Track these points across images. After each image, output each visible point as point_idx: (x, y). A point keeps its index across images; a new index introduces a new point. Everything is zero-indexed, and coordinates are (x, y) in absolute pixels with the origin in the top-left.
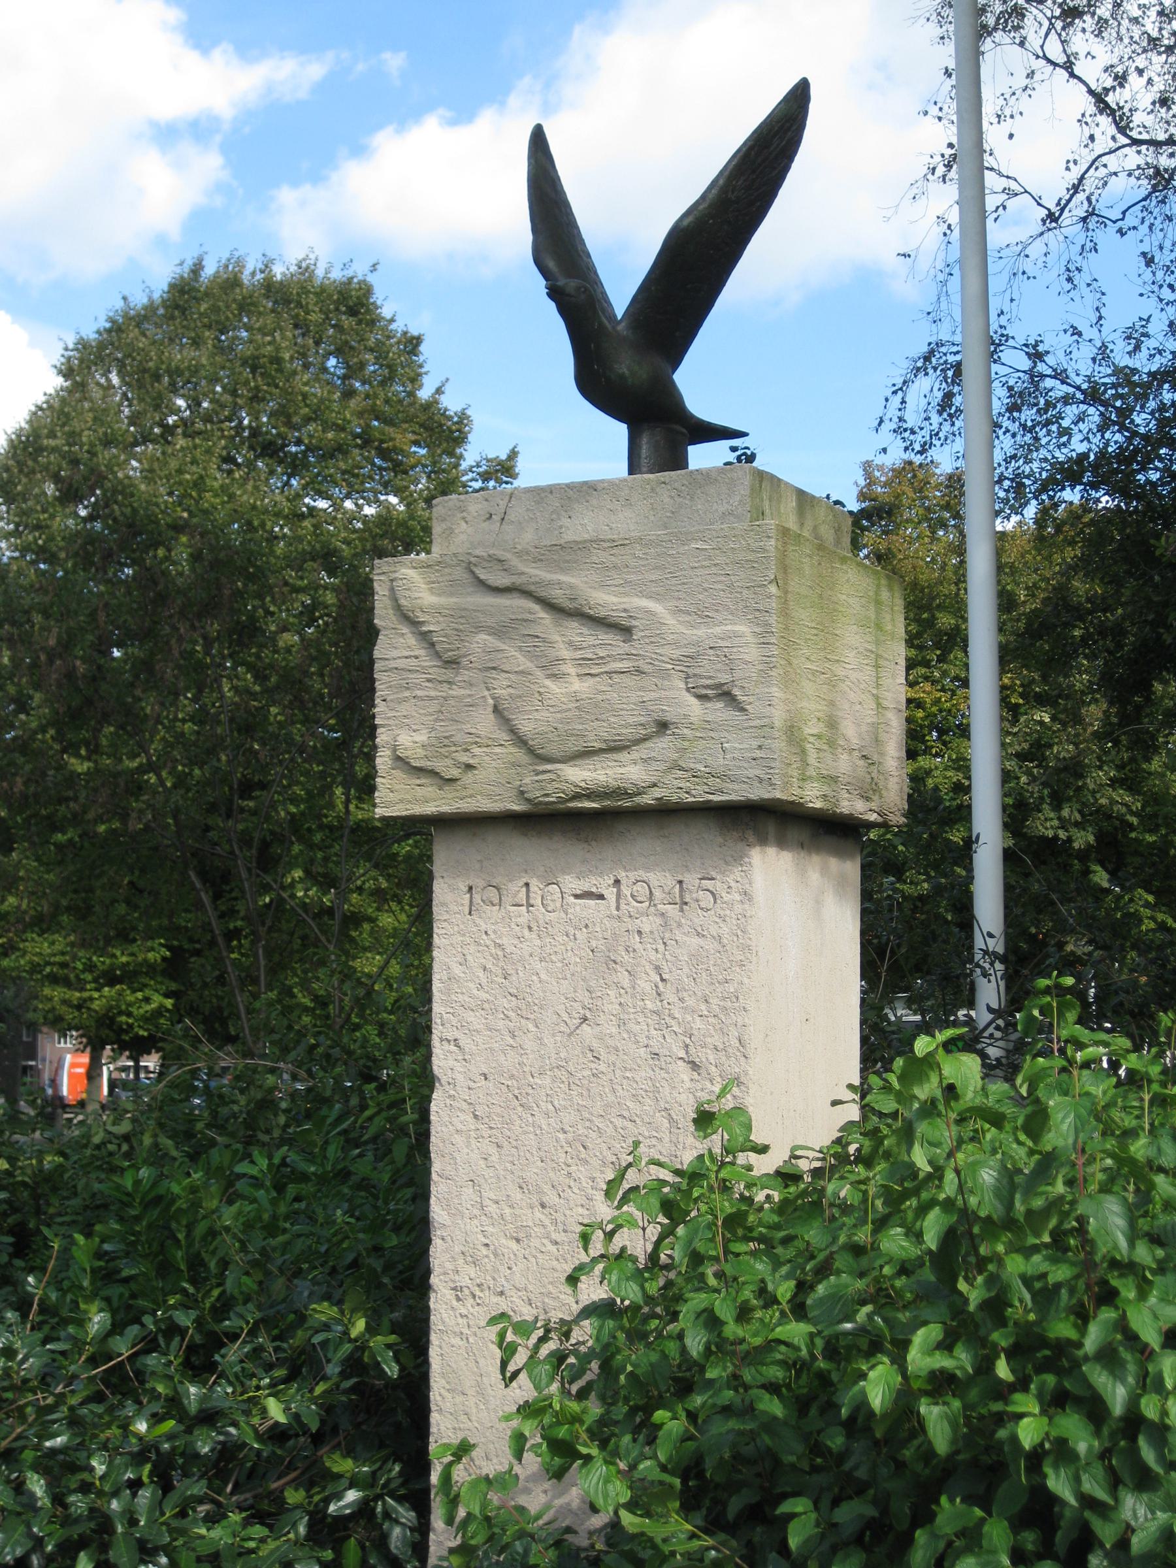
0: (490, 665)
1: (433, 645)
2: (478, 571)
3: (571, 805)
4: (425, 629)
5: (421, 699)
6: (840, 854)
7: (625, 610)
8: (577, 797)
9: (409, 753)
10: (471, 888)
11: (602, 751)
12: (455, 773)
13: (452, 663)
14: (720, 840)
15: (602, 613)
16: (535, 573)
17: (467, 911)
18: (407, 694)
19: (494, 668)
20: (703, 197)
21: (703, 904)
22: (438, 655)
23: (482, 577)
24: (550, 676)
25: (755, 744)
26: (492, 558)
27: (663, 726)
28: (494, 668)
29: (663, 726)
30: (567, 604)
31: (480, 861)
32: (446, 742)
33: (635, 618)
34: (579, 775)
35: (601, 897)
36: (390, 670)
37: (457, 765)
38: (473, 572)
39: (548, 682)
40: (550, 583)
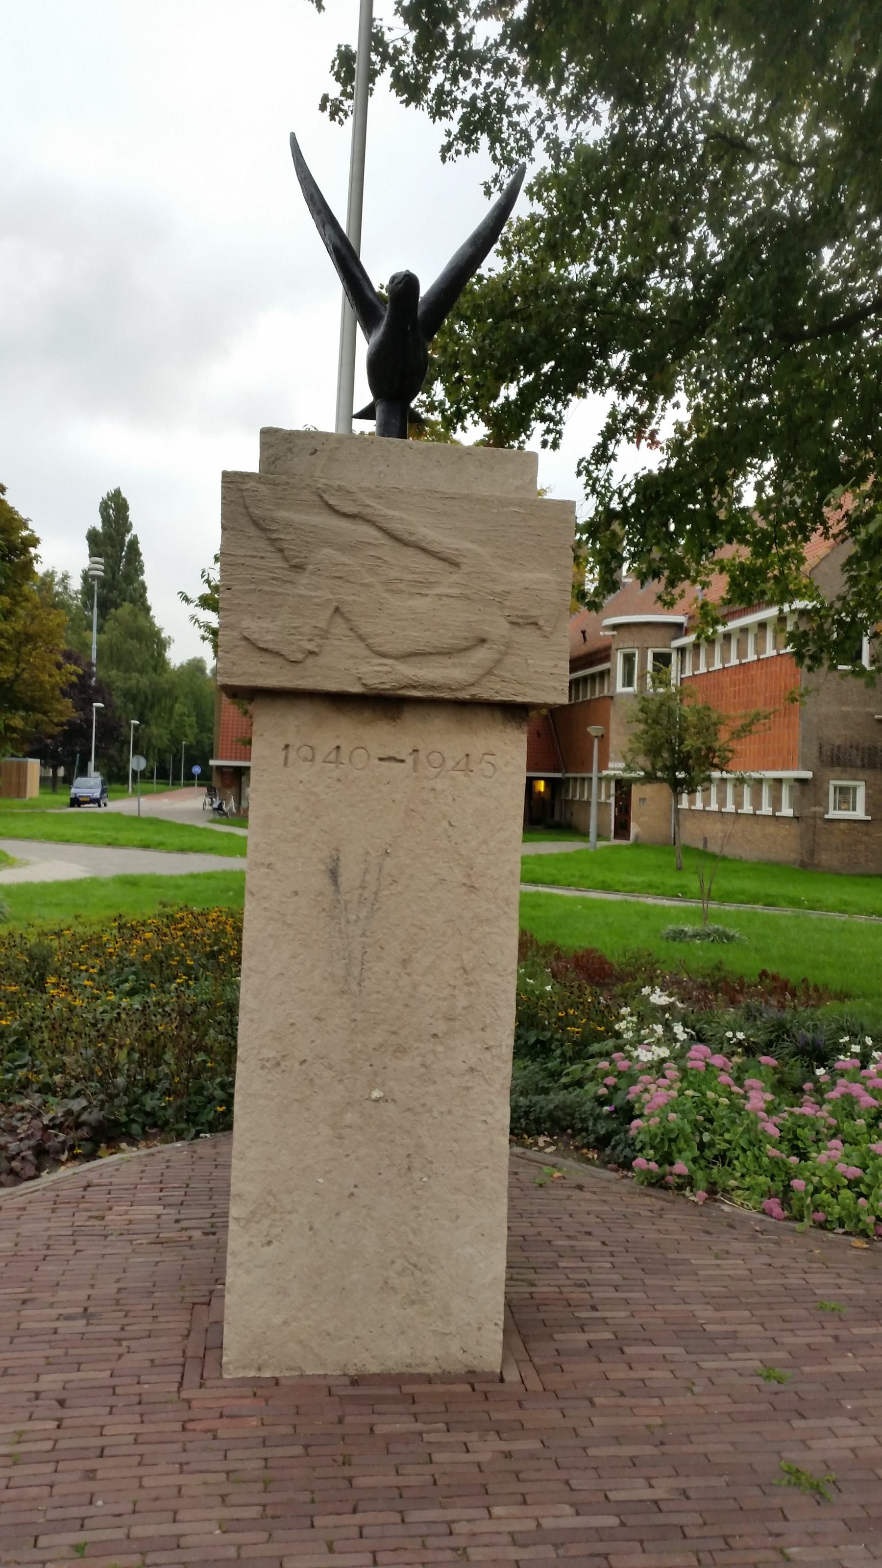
0: (337, 575)
1: (281, 550)
2: (326, 497)
3: (400, 692)
4: (274, 536)
5: (267, 593)
6: (520, 727)
7: (457, 550)
8: (404, 687)
9: (256, 636)
10: (287, 746)
11: (431, 654)
12: (300, 656)
13: (299, 568)
14: (501, 727)
15: (437, 549)
16: (379, 509)
17: (282, 762)
18: (252, 587)
19: (340, 578)
20: (484, 222)
21: (486, 773)
22: (286, 559)
23: (331, 502)
24: (388, 591)
25: (552, 663)
26: (340, 488)
27: (483, 641)
28: (340, 578)
29: (483, 641)
30: (406, 537)
31: (297, 726)
32: (293, 631)
33: (465, 557)
34: (409, 671)
35: (402, 761)
36: (237, 565)
37: (302, 651)
38: (321, 497)
39: (386, 595)
40: (392, 518)
